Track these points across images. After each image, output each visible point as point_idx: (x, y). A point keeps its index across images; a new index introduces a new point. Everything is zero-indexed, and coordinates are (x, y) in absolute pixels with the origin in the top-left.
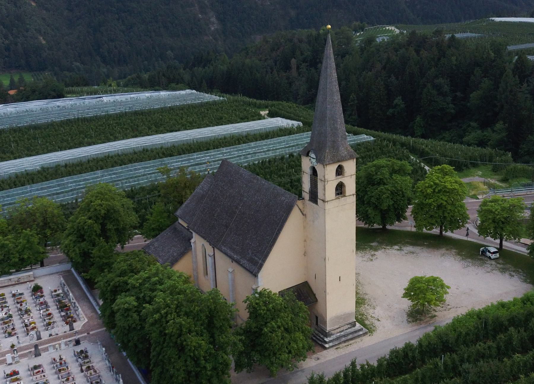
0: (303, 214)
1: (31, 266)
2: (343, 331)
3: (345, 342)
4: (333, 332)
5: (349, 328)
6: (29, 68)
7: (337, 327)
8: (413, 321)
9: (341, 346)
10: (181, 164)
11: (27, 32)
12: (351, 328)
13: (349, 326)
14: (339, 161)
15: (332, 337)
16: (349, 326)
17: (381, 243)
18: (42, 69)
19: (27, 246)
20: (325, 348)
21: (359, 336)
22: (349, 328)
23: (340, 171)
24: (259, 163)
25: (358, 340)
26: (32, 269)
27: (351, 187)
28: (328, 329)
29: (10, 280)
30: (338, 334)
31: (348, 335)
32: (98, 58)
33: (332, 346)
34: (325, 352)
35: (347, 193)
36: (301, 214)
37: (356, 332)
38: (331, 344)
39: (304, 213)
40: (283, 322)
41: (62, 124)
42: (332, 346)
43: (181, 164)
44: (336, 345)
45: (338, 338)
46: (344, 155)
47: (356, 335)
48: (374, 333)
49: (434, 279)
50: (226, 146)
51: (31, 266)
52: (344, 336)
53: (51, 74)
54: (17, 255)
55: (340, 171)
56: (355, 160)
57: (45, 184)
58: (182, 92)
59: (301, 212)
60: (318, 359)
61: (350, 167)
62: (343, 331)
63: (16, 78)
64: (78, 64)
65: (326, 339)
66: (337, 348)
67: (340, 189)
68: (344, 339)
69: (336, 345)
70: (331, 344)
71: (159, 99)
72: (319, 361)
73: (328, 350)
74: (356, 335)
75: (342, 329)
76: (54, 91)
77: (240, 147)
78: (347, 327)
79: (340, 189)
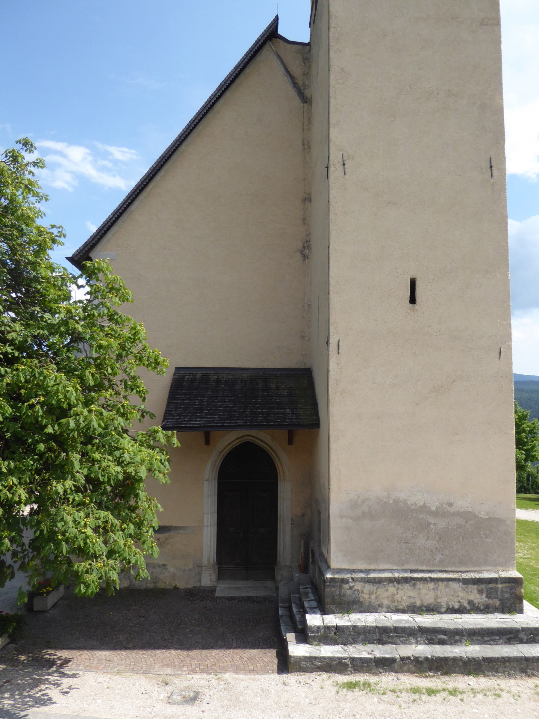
4: (366, 592)
5: (474, 609)
12: (486, 610)
20: (285, 664)
36: (292, 92)
39: (307, 93)
59: (295, 83)
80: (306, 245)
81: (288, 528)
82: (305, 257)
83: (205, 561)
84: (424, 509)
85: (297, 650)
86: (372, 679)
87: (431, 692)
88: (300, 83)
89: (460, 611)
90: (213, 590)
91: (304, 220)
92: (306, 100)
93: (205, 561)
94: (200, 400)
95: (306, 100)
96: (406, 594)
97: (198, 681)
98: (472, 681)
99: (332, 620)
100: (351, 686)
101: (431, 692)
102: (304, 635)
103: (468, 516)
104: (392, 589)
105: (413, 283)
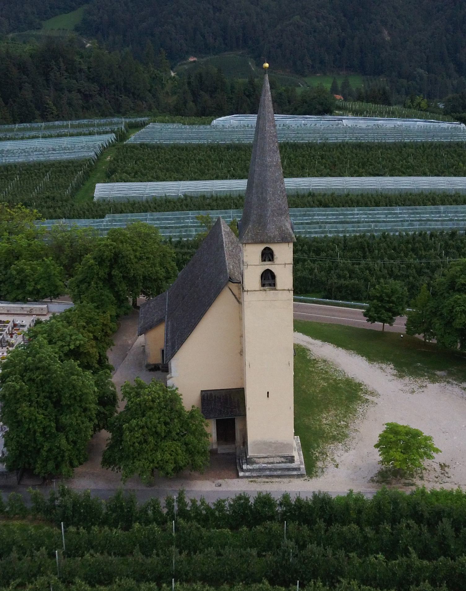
0: (238, 301)
1: (51, 299)
2: (272, 463)
3: (267, 477)
4: (257, 460)
5: (282, 462)
6: (362, 69)
7: (265, 455)
8: (378, 482)
9: (259, 480)
10: (344, 218)
11: (371, 23)
12: (286, 462)
13: (283, 460)
14: (267, 242)
15: (254, 465)
16: (283, 460)
17: (450, 374)
18: (377, 72)
19: (43, 275)
20: (238, 477)
21: (293, 476)
22: (282, 462)
23: (267, 255)
24: (415, 234)
25: (286, 480)
26: (51, 302)
27: (285, 277)
28: (250, 454)
29: (22, 308)
30: (264, 465)
31: (276, 470)
32: (452, 65)
33: (248, 477)
34: (235, 481)
35: (279, 285)
36: (235, 301)
37: (289, 469)
38: (247, 474)
39: (240, 300)
40: (148, 423)
41: (228, 147)
42: (248, 477)
43: (327, 219)
44: (253, 477)
45: (260, 470)
46: (272, 235)
47: (287, 473)
48: (314, 479)
49: (415, 434)
50: (358, 206)
51: (51, 299)
52: (270, 469)
53: (387, 80)
54: (33, 283)
55: (267, 255)
56: (291, 245)
57: (157, 215)
58: (445, 125)
59: (236, 298)
60: (220, 485)
61: (284, 254)
62: (272, 463)
63: (340, 83)
64: (421, 71)
65: (245, 467)
66: (252, 481)
67: (268, 279)
68: (268, 473)
69: (253, 477)
70: (247, 474)
71: (408, 130)
72: (220, 489)
73: (240, 480)
74: (287, 473)
75: (271, 460)
76: (322, 104)
77: (420, 209)
78: (279, 459)
79: (268, 279)
80: (241, 200)
81: (239, 432)
82: (241, 355)
83: (214, 441)
84: (271, 442)
85: (241, 474)
86: (256, 480)
87: (267, 482)
88: (238, 297)
89: (279, 463)
90: (217, 450)
91: (241, 343)
92: (239, 302)
93: (214, 441)
94: (209, 399)
95: (239, 302)
96: (266, 460)
97: (220, 481)
98: (277, 480)
99: (249, 467)
100: (252, 481)
101: (267, 482)
102: (242, 470)
103: (281, 443)
104: (263, 459)
105: (268, 393)
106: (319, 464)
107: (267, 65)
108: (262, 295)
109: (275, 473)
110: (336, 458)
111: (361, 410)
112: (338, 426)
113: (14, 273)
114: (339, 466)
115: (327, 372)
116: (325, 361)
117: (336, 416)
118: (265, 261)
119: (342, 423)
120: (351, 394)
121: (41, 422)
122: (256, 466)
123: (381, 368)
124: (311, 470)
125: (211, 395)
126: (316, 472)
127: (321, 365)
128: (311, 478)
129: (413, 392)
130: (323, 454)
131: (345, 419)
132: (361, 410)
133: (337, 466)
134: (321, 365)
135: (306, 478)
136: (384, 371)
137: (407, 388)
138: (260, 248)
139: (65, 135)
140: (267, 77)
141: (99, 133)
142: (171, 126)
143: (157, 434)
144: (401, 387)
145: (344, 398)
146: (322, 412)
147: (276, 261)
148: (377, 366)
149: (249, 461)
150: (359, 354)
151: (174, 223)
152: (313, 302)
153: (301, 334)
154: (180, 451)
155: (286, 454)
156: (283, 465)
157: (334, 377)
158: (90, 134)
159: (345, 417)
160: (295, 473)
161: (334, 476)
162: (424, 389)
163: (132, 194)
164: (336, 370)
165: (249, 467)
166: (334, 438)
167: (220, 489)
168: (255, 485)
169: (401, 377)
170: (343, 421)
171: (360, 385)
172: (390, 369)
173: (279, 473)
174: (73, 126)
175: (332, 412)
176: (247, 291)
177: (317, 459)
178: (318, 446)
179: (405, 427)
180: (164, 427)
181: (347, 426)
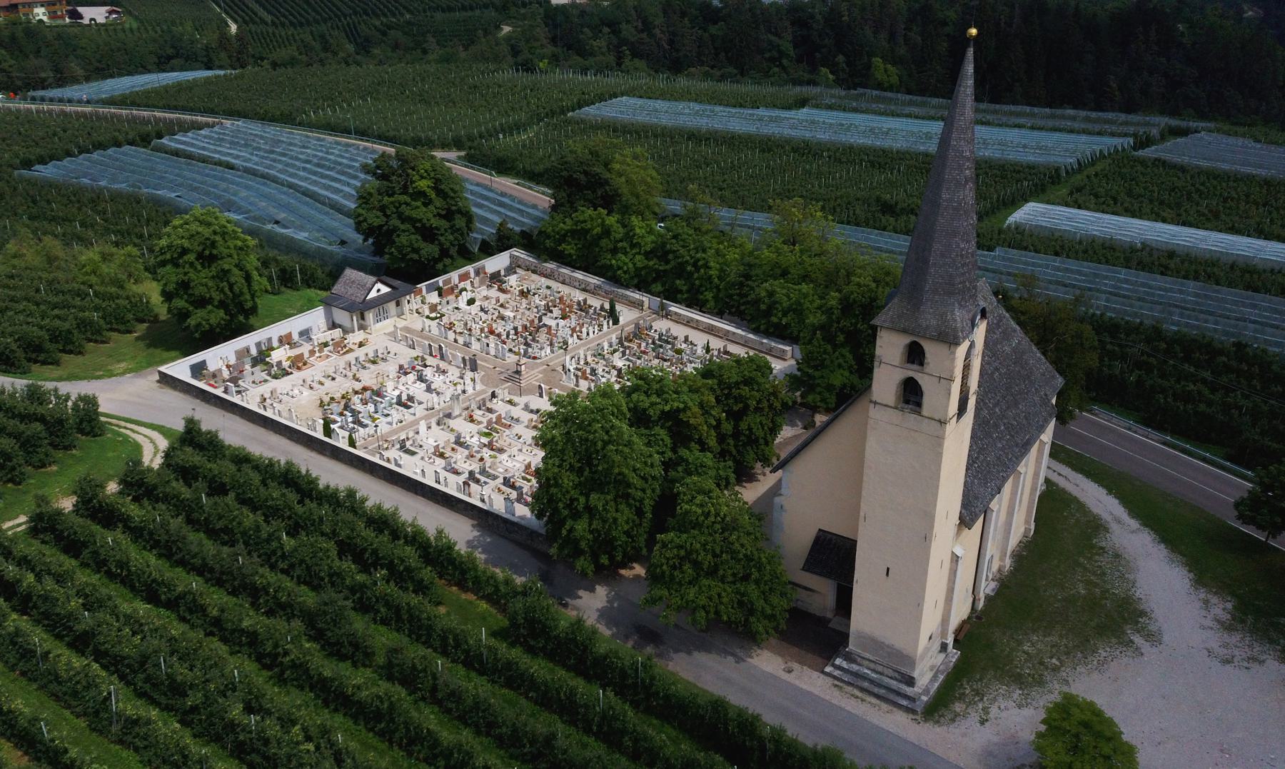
3: (862, 690)
5: (896, 679)
9: (850, 689)
16: (896, 675)
20: (823, 672)
21: (900, 707)
25: (885, 706)
28: (851, 647)
31: (880, 685)
34: (816, 674)
37: (898, 694)
38: (837, 673)
47: (892, 697)
52: (872, 681)
60: (790, 671)
62: (881, 674)
68: (866, 684)
70: (837, 673)
72: (785, 676)
73: (822, 676)
74: (892, 697)
75: (880, 668)
78: (890, 672)
90: (830, 621)
96: (872, 666)
97: (796, 666)
98: (874, 700)
99: (845, 665)
106: (958, 707)
107: (974, 31)
108: (895, 416)
109: (876, 690)
110: (994, 711)
111: (1104, 654)
112: (1041, 663)
113: (763, 294)
114: (987, 724)
115: (1104, 574)
116: (1117, 556)
117: (1053, 646)
118: (913, 362)
119: (1054, 661)
120: (1115, 620)
121: (568, 492)
122: (855, 667)
123: (1206, 602)
124: (937, 708)
125: (831, 540)
126: (943, 716)
127: (1103, 561)
128: (926, 721)
129: (1227, 662)
130: (978, 694)
131: (1064, 658)
132: (1104, 654)
133: (982, 722)
134: (1103, 561)
135: (918, 718)
136: (1207, 609)
137: (1222, 651)
138: (905, 340)
139: (1060, 130)
140: (970, 53)
141: (1113, 135)
142: (1232, 140)
143: (696, 565)
144: (1214, 644)
145: (1093, 624)
146: (1034, 631)
147: (928, 369)
148: (1202, 596)
149: (849, 658)
150: (1187, 565)
151: (1084, 281)
152: (1204, 460)
153: (1117, 501)
154: (725, 600)
155: (903, 670)
156: (894, 684)
157: (1109, 587)
158: (1099, 134)
159: (1067, 654)
160: (904, 703)
161: (964, 735)
162: (1255, 666)
163: (1065, 226)
164: (1122, 577)
165: (845, 665)
166: (1019, 680)
167: (785, 676)
168: (836, 693)
169: (1228, 628)
170: (1059, 659)
171: (1143, 613)
172: (1221, 608)
173: (882, 692)
174: (1087, 119)
175: (1055, 639)
176: (875, 403)
177: (962, 697)
178: (981, 680)
179: (741, 712)
180: (709, 557)
181: (1056, 669)
